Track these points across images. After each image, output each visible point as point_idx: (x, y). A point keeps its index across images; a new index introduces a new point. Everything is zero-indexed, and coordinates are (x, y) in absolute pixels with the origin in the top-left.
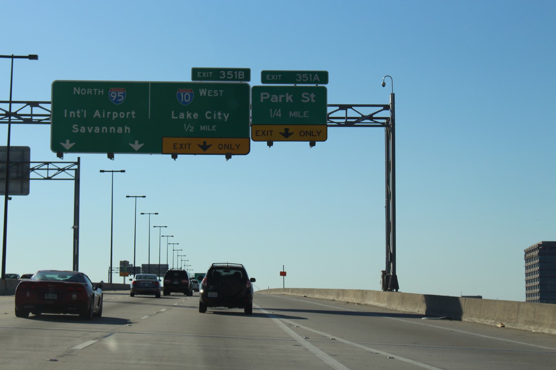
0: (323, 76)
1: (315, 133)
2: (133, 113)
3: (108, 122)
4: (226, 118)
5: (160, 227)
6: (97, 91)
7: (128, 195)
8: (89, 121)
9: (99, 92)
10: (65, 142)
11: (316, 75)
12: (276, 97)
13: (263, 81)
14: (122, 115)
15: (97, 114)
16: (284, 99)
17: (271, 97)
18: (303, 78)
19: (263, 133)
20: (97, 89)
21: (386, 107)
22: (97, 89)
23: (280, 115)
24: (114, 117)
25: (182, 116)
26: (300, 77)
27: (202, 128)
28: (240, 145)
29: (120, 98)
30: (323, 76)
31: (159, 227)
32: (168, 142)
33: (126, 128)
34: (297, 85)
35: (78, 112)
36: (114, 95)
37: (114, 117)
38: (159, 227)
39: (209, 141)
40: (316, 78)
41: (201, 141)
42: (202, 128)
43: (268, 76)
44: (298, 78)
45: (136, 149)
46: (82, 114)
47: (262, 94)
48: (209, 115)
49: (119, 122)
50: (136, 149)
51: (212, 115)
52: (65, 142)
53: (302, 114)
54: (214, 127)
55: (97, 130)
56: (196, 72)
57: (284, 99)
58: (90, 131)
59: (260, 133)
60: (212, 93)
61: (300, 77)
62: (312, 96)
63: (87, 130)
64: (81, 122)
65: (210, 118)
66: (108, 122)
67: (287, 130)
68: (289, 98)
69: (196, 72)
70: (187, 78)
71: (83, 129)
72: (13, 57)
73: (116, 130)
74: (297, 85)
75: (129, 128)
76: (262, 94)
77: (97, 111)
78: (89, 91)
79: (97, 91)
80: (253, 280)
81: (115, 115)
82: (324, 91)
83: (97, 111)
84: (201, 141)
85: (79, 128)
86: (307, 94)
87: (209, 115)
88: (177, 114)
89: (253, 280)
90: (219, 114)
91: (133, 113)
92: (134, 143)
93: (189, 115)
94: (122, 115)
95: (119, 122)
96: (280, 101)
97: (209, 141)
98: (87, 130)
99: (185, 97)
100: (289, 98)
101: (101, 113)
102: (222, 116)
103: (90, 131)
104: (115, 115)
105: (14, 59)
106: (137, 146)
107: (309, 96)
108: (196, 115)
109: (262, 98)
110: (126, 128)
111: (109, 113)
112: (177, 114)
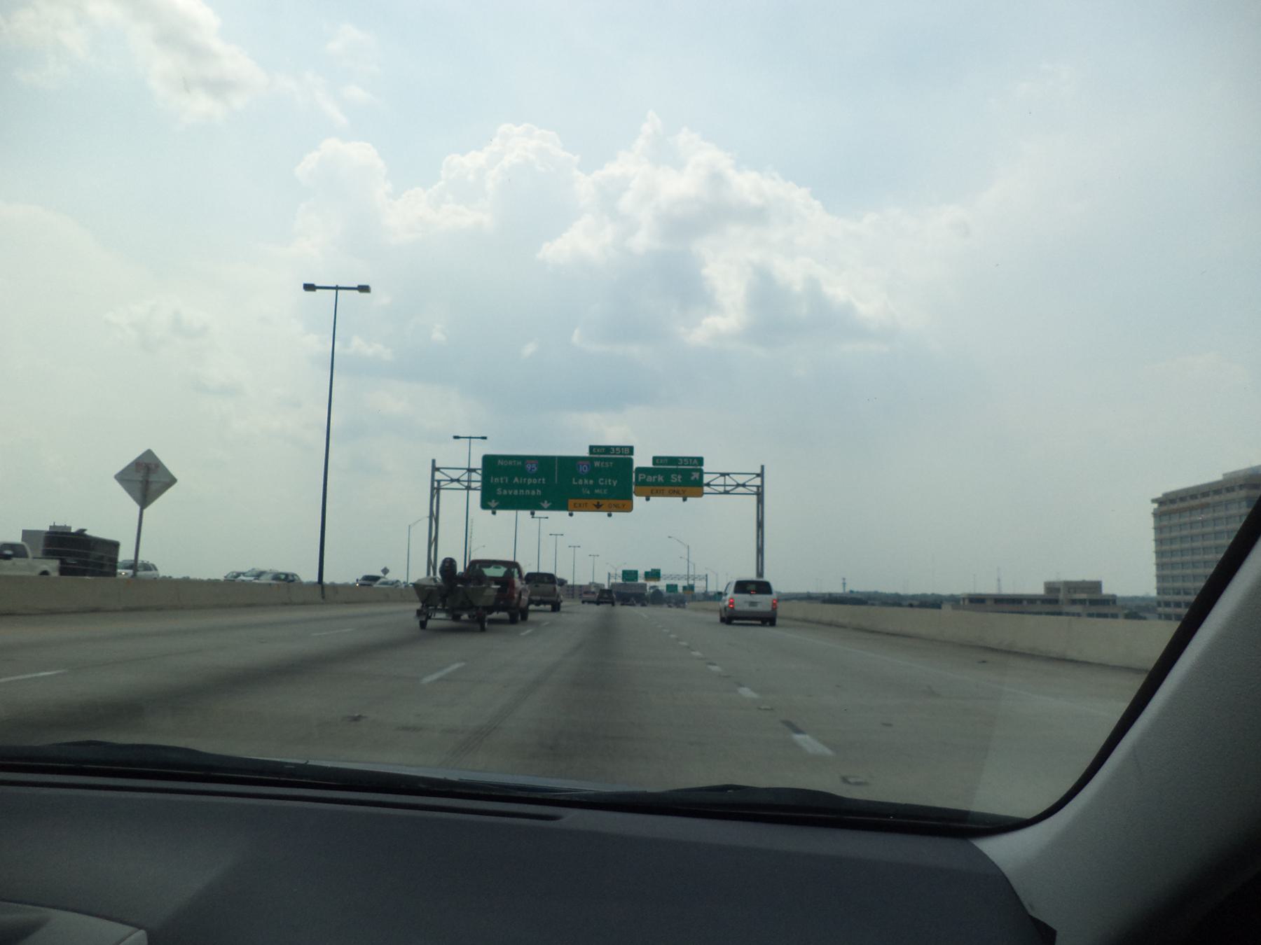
0: (631, 450)
1: (681, 492)
2: (543, 480)
3: (523, 486)
5: (468, 440)
7: (456, 435)
8: (510, 486)
13: (654, 464)
14: (535, 481)
15: (516, 480)
16: (656, 479)
17: (646, 478)
24: (529, 483)
25: (580, 482)
26: (613, 450)
27: (597, 491)
28: (763, 467)
30: (631, 450)
31: (466, 438)
32: (571, 502)
33: (538, 491)
34: (679, 467)
35: (502, 479)
36: (529, 467)
37: (529, 483)
38: (466, 438)
39: (601, 502)
40: (695, 462)
41: (595, 502)
42: (597, 491)
43: (594, 450)
45: (546, 507)
46: (504, 480)
47: (640, 475)
48: (602, 482)
49: (532, 487)
50: (546, 507)
51: (604, 481)
54: (679, 477)
55: (516, 492)
56: (592, 448)
57: (656, 479)
59: (577, 505)
60: (604, 465)
61: (613, 450)
62: (679, 477)
63: (508, 492)
64: (504, 486)
65: (602, 484)
66: (523, 486)
67: (598, 503)
68: (660, 479)
69: (592, 448)
70: (585, 452)
71: (505, 492)
72: (337, 288)
73: (531, 492)
76: (640, 475)
78: (510, 463)
80: (610, 515)
81: (530, 481)
84: (595, 502)
85: (502, 491)
86: (676, 475)
87: (602, 482)
89: (610, 515)
91: (543, 480)
92: (544, 502)
93: (586, 481)
94: (535, 481)
95: (532, 487)
96: (654, 480)
97: (601, 502)
98: (508, 492)
99: (584, 469)
100: (660, 479)
101: (519, 480)
102: (612, 482)
104: (530, 481)
105: (339, 291)
106: (546, 505)
107: (676, 477)
108: (591, 482)
109: (640, 478)
110: (538, 491)
111: (525, 479)
112: (576, 481)
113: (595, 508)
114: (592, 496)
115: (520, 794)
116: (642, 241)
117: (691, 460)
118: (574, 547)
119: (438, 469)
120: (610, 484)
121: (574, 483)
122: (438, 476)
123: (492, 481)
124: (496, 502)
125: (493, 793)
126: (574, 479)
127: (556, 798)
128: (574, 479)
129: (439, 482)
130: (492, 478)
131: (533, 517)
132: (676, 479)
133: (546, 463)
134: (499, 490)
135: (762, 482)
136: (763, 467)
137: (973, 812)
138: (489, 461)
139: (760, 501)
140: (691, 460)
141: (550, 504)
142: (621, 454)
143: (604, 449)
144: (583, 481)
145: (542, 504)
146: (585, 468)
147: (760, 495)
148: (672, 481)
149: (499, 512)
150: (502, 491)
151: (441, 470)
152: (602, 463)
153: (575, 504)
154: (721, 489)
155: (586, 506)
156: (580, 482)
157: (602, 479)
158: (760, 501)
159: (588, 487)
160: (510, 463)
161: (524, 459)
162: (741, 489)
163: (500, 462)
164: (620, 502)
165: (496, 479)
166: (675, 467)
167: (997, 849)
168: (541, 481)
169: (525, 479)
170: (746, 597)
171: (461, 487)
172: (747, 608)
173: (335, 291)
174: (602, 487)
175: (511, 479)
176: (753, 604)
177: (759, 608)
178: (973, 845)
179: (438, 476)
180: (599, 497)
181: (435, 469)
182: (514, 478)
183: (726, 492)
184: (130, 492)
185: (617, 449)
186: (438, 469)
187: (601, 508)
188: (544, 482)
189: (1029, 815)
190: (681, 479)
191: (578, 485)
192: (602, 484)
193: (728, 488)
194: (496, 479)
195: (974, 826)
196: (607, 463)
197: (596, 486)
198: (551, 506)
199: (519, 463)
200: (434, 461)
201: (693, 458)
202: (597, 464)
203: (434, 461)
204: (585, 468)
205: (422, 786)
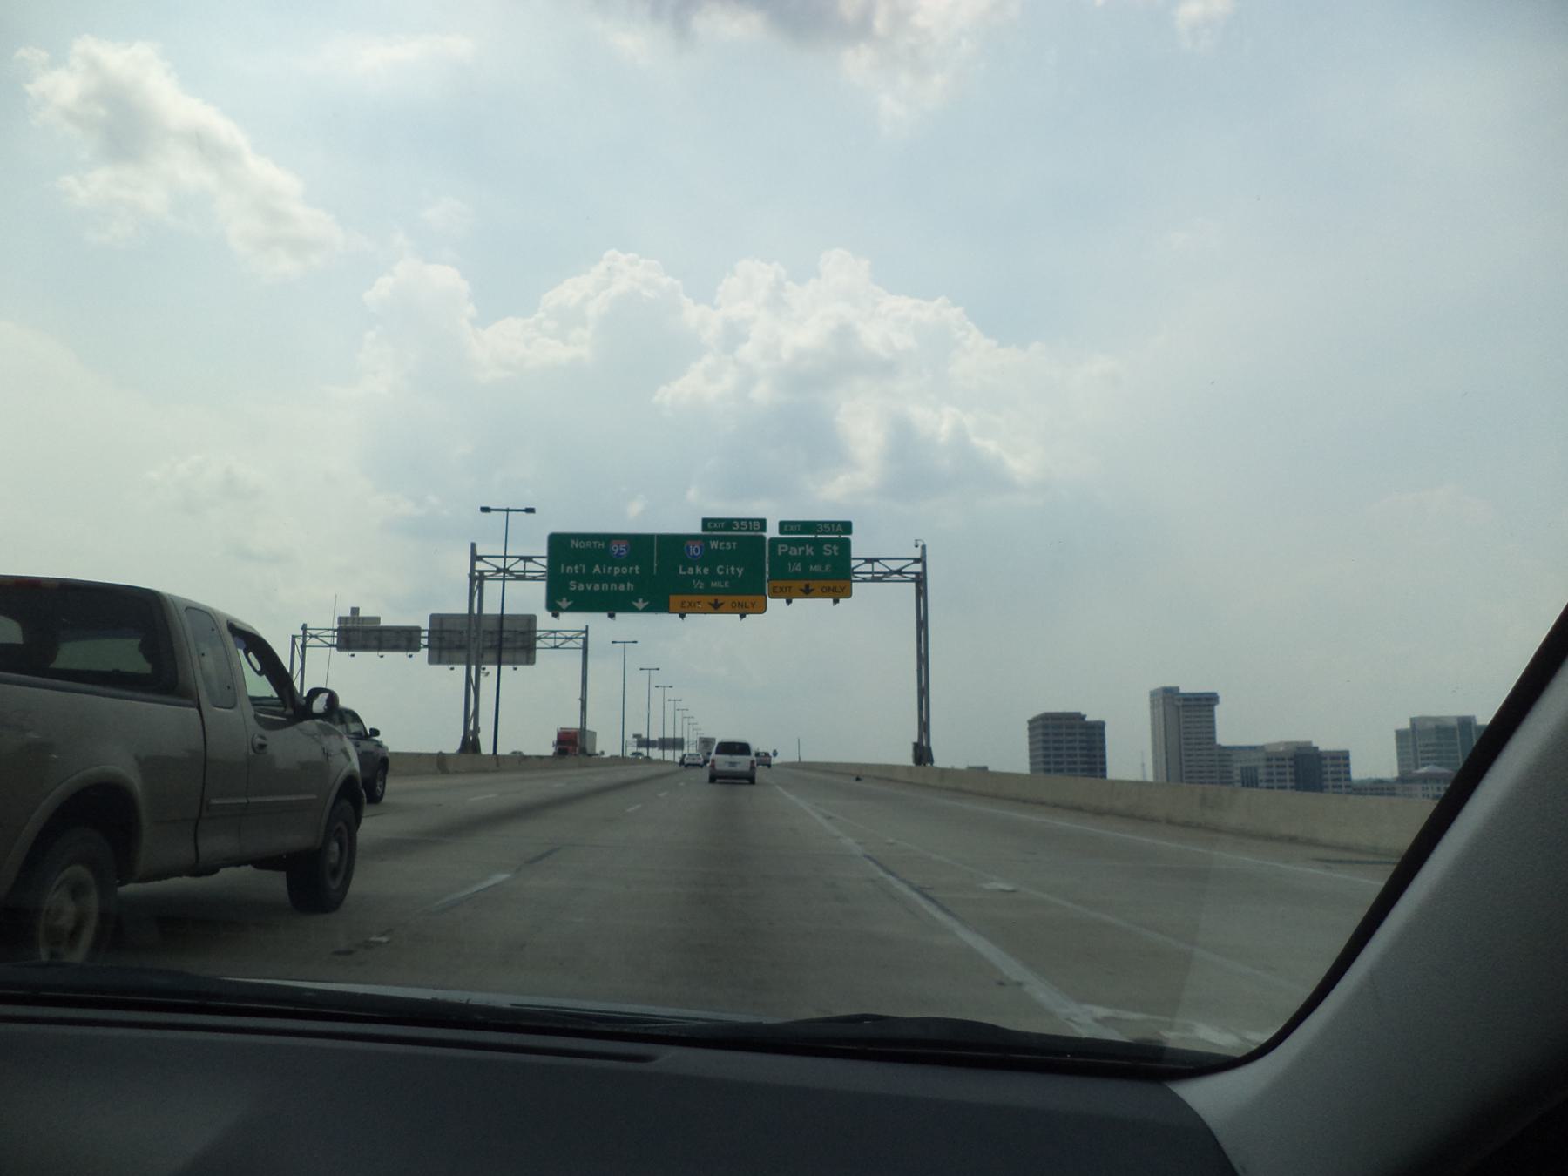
0: (847, 527)
2: (637, 568)
3: (609, 578)
4: (740, 573)
6: (597, 544)
8: (589, 578)
9: (600, 545)
10: (637, 601)
11: (839, 525)
12: (795, 550)
13: (781, 532)
14: (624, 570)
15: (597, 569)
16: (804, 552)
17: (789, 550)
18: (740, 526)
19: (690, 604)
20: (803, 548)
21: (917, 561)
22: (803, 548)
23: (800, 570)
24: (616, 573)
25: (691, 571)
26: (821, 528)
27: (713, 584)
28: (587, 627)
29: (623, 551)
32: (675, 600)
33: (629, 584)
34: (819, 536)
35: (576, 567)
36: (615, 548)
37: (616, 573)
40: (839, 528)
41: (711, 599)
42: (713, 584)
43: (786, 527)
44: (818, 528)
46: (580, 570)
47: (780, 546)
49: (621, 579)
51: (725, 570)
52: (637, 601)
53: (823, 569)
55: (597, 587)
56: (706, 523)
57: (804, 552)
58: (589, 588)
59: (778, 590)
61: (821, 528)
63: (585, 587)
64: (578, 578)
65: (721, 573)
66: (609, 578)
67: (716, 601)
68: (809, 551)
69: (706, 523)
70: (696, 528)
71: (581, 587)
74: (819, 536)
75: (632, 586)
76: (780, 546)
77: (597, 566)
78: (589, 544)
79: (597, 544)
81: (617, 571)
82: (847, 543)
83: (597, 566)
84: (802, 584)
85: (577, 585)
86: (830, 546)
87: (721, 570)
88: (685, 569)
90: (733, 569)
92: (561, 601)
93: (698, 570)
94: (624, 570)
95: (621, 579)
96: (800, 553)
97: (721, 599)
98: (585, 587)
99: (694, 550)
100: (809, 551)
102: (736, 571)
103: (589, 588)
104: (617, 571)
106: (640, 604)
107: (830, 548)
108: (706, 571)
111: (610, 568)
112: (685, 569)
113: (712, 609)
114: (708, 591)
115: (602, 1027)
116: (761, 392)
117: (833, 526)
118: (664, 687)
119: (480, 558)
120: (733, 573)
121: (681, 572)
122: (480, 566)
123: (562, 571)
124: (568, 601)
125: (570, 1026)
126: (681, 568)
127: (649, 1031)
128: (681, 568)
129: (481, 572)
130: (562, 566)
131: (682, 607)
132: (830, 551)
133: (639, 545)
134: (572, 583)
135: (587, 635)
136: (587, 627)
137: (1173, 1049)
138: (559, 544)
139: (921, 593)
140: (833, 526)
141: (570, 603)
142: (748, 530)
143: (799, 526)
144: (695, 570)
145: (635, 603)
146: (697, 549)
147: (920, 581)
148: (825, 553)
149: (618, 615)
150: (577, 585)
151: (534, 559)
152: (721, 544)
153: (683, 603)
154: (558, 635)
155: (790, 591)
156: (691, 571)
157: (721, 567)
158: (921, 593)
159: (701, 577)
160: (589, 544)
161: (608, 538)
162: (569, 634)
163: (575, 544)
164: (751, 598)
165: (568, 568)
166: (813, 536)
167: (1200, 1095)
168: (634, 571)
169: (610, 568)
170: (727, 758)
171: (513, 577)
172: (726, 768)
173: (505, 513)
174: (722, 579)
175: (590, 567)
176: (733, 764)
177: (739, 768)
178: (1169, 1089)
179: (480, 566)
180: (717, 591)
181: (475, 558)
182: (594, 566)
183: (554, 632)
184: (195, 610)
185: (825, 526)
186: (480, 558)
187: (721, 609)
188: (637, 572)
189: (1239, 1054)
190: (837, 551)
191: (687, 574)
192: (721, 573)
193: (553, 635)
194: (569, 568)
195: (1172, 1066)
196: (728, 544)
197: (713, 576)
198: (571, 605)
199: (602, 545)
200: (473, 546)
201: (836, 523)
202: (714, 545)
203: (473, 546)
204: (697, 550)
205: (480, 1018)
